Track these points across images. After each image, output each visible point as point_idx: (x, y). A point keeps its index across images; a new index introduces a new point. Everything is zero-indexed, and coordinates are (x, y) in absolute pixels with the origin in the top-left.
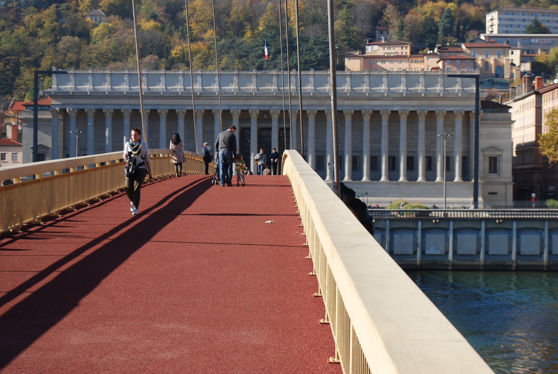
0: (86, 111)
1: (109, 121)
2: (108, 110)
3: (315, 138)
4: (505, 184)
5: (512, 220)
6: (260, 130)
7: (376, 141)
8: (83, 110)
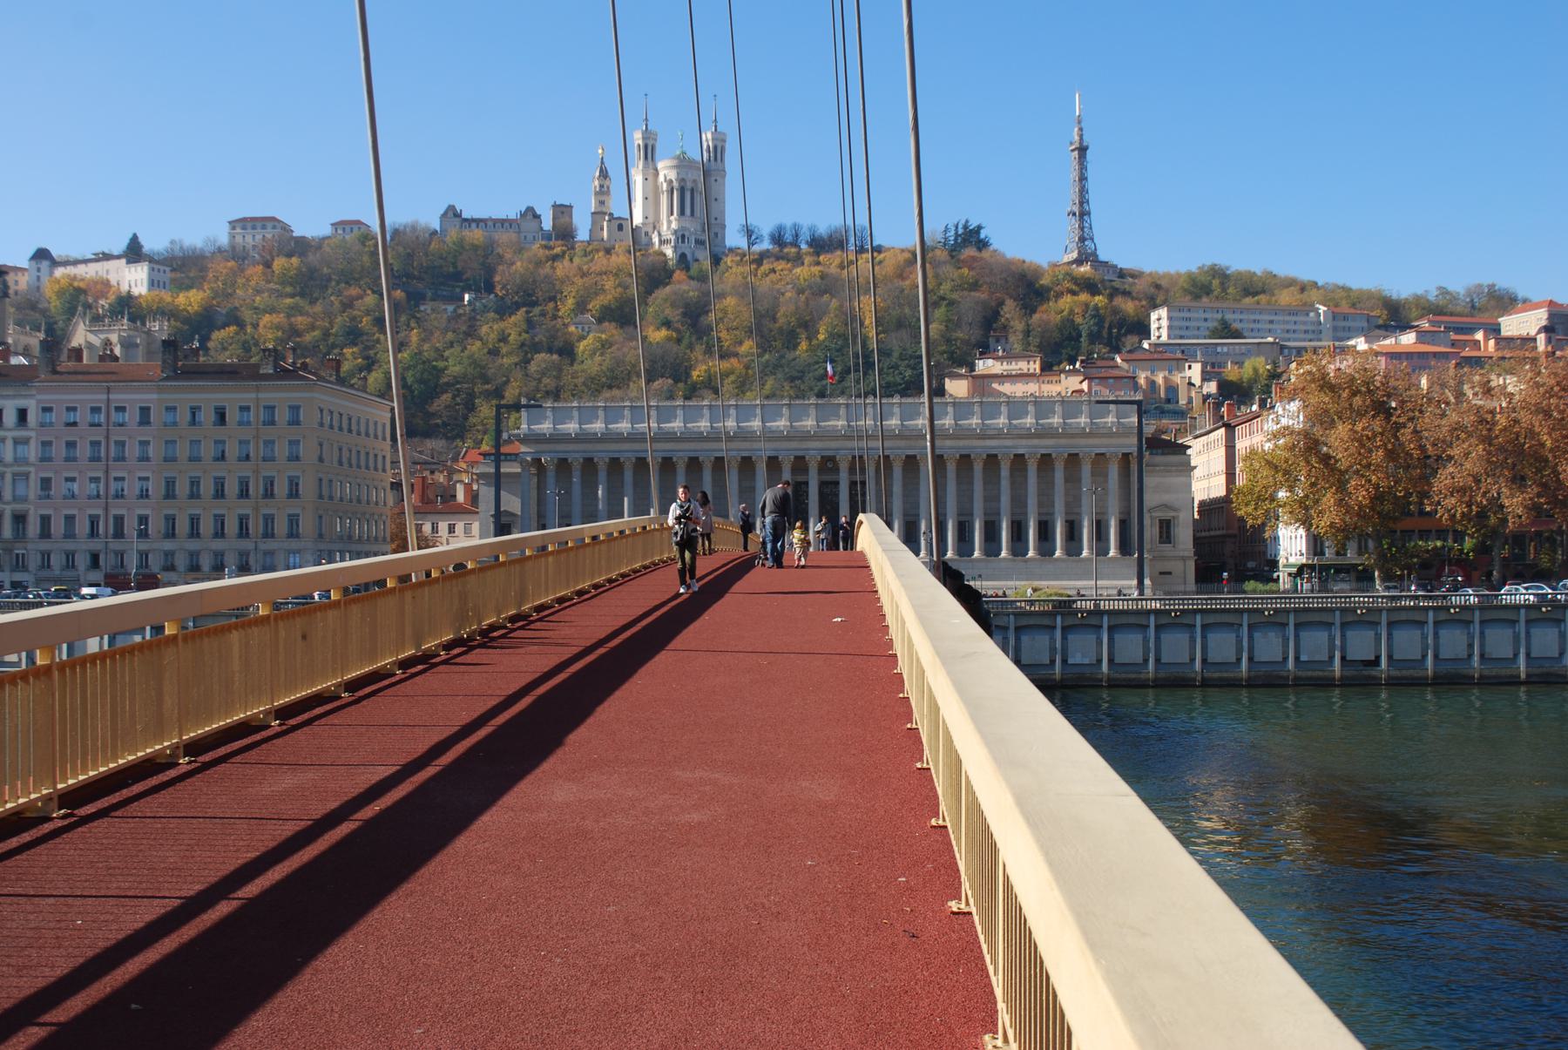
1: (602, 476)
4: (1184, 559)
6: (822, 484)
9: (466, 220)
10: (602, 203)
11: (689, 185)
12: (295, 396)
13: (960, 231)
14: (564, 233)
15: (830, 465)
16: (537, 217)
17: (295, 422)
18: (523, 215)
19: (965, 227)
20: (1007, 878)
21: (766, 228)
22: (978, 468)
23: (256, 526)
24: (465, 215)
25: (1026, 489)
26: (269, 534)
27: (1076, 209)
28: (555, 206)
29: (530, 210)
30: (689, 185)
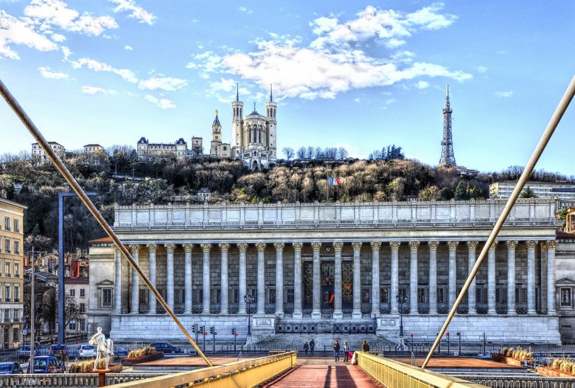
0: (147, 246)
1: (206, 257)
2: (170, 246)
3: (283, 276)
5: (568, 354)
6: (323, 263)
7: (404, 274)
8: (145, 245)
9: (150, 145)
10: (217, 137)
11: (258, 127)
13: (390, 151)
14: (198, 149)
16: (184, 143)
18: (178, 143)
19: (393, 148)
20: (334, 298)
21: (296, 150)
22: (433, 252)
24: (150, 142)
27: (445, 141)
28: (193, 138)
29: (181, 140)
30: (258, 127)
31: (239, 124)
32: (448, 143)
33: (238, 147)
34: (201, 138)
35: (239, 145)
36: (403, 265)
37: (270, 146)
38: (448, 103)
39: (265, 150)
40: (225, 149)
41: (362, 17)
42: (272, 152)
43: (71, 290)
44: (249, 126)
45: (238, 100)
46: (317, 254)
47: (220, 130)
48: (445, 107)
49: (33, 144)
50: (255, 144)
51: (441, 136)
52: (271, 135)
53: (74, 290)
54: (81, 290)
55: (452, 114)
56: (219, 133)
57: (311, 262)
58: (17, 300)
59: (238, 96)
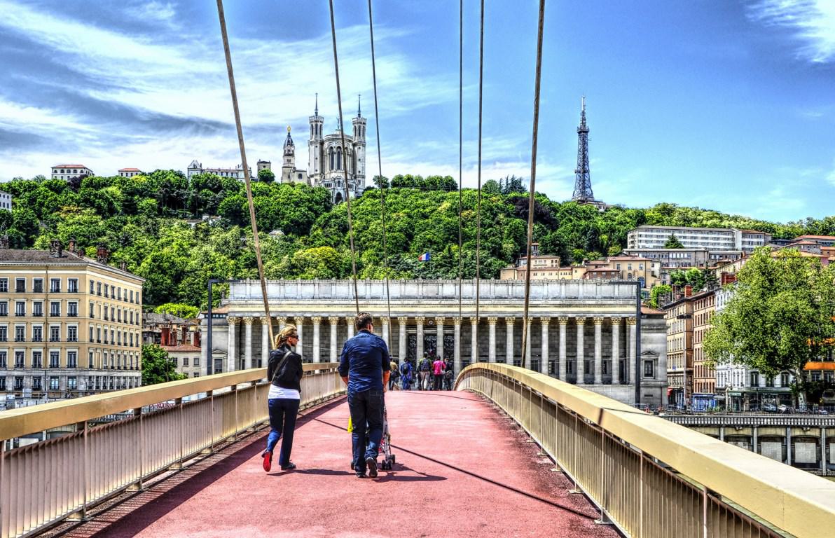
10: (289, 161)
12: (73, 273)
13: (510, 182)
14: (267, 178)
15: (431, 322)
17: (73, 314)
19: (513, 179)
23: (46, 335)
25: (558, 340)
26: (55, 366)
31: (318, 145)
32: (583, 171)
33: (316, 175)
34: (269, 163)
35: (318, 172)
36: (500, 338)
37: (358, 174)
38: (584, 119)
39: (352, 179)
40: (300, 176)
41: (429, 535)
42: (359, 181)
43: (185, 359)
44: (332, 148)
45: (317, 115)
46: (420, 327)
47: (293, 151)
48: (579, 124)
49: (53, 168)
50: (339, 171)
51: (574, 162)
52: (359, 160)
53: (187, 359)
54: (185, 359)
55: (588, 134)
56: (292, 155)
57: (415, 335)
58: (137, 369)
59: (316, 109)
